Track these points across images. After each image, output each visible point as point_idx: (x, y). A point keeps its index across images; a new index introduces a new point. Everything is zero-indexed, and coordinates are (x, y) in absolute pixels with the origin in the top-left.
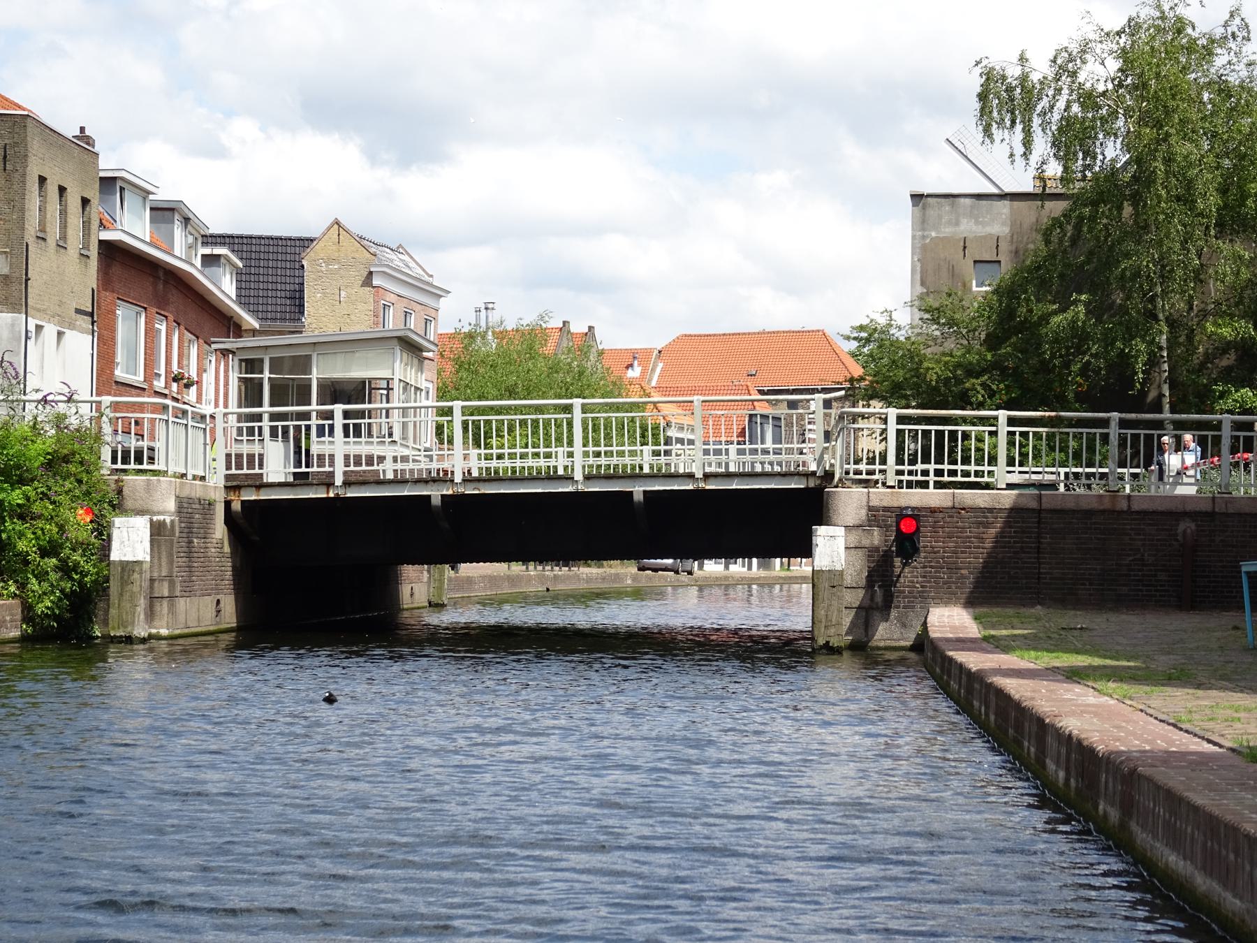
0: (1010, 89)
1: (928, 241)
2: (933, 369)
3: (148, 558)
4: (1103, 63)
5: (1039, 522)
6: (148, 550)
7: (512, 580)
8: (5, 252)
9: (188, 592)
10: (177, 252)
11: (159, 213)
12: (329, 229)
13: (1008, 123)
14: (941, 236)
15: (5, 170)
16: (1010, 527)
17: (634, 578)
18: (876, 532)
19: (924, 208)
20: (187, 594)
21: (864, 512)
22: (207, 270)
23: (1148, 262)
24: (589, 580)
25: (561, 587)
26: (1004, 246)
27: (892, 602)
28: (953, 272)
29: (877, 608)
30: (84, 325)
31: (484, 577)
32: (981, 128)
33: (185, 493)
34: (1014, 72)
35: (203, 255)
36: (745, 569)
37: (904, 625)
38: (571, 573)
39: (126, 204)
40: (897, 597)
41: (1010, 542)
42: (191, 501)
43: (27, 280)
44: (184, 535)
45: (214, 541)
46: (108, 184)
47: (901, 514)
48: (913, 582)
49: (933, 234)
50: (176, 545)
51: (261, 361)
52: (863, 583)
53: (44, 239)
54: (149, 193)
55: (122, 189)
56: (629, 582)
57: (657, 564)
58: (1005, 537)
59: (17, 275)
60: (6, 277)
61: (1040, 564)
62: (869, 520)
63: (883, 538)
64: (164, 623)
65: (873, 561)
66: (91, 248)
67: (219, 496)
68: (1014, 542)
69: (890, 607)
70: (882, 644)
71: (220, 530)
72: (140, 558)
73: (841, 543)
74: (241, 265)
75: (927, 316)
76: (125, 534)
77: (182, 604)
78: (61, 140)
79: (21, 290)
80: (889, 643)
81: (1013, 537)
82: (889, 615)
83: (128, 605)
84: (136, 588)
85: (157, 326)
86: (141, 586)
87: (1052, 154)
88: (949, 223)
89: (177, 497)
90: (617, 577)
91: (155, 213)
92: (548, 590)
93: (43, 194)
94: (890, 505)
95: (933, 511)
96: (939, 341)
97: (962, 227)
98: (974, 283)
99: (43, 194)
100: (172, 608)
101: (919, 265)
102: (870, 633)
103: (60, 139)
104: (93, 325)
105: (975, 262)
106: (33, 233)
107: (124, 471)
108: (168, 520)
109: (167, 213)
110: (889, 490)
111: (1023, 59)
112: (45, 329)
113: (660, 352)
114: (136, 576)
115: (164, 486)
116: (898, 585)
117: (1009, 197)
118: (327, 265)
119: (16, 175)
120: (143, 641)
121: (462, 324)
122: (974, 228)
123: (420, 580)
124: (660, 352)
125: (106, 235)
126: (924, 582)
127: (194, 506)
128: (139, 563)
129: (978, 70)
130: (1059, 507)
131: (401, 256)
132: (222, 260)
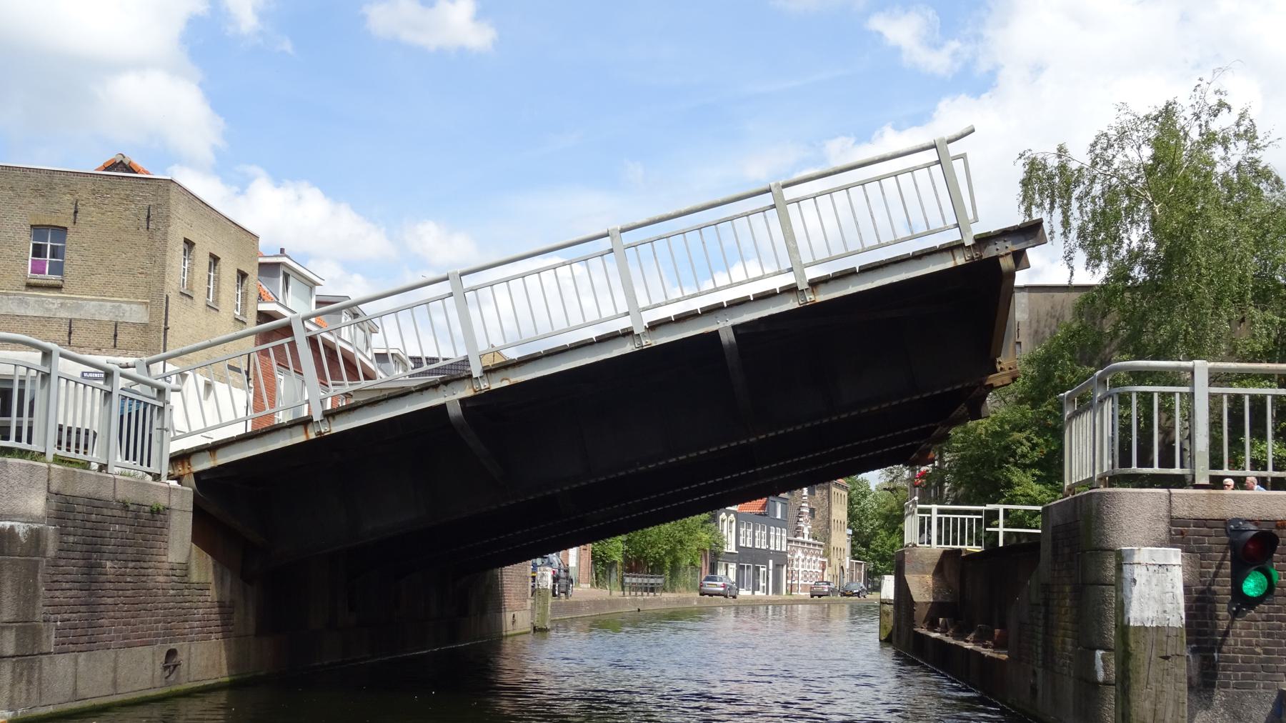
0: (1051, 177)
7: (612, 603)
8: (146, 303)
13: (1047, 206)
15: (148, 228)
17: (699, 601)
23: (1187, 326)
24: (668, 602)
27: (1215, 676)
31: (589, 602)
32: (1023, 208)
33: (85, 486)
34: (1053, 162)
36: (765, 594)
38: (656, 598)
39: (290, 287)
40: (1225, 669)
43: (166, 329)
48: (1249, 644)
53: (191, 297)
54: (315, 284)
55: (286, 276)
56: (695, 603)
57: (712, 591)
59: (156, 323)
60: (146, 325)
66: (248, 315)
69: (1213, 685)
78: (214, 215)
79: (159, 338)
82: (1210, 699)
87: (1078, 244)
90: (687, 600)
92: (639, 610)
93: (191, 257)
94: (1207, 515)
103: (213, 213)
106: (175, 287)
108: (21, 528)
111: (1061, 151)
116: (1225, 648)
117: (1027, 289)
119: (159, 233)
123: (522, 608)
129: (1022, 161)
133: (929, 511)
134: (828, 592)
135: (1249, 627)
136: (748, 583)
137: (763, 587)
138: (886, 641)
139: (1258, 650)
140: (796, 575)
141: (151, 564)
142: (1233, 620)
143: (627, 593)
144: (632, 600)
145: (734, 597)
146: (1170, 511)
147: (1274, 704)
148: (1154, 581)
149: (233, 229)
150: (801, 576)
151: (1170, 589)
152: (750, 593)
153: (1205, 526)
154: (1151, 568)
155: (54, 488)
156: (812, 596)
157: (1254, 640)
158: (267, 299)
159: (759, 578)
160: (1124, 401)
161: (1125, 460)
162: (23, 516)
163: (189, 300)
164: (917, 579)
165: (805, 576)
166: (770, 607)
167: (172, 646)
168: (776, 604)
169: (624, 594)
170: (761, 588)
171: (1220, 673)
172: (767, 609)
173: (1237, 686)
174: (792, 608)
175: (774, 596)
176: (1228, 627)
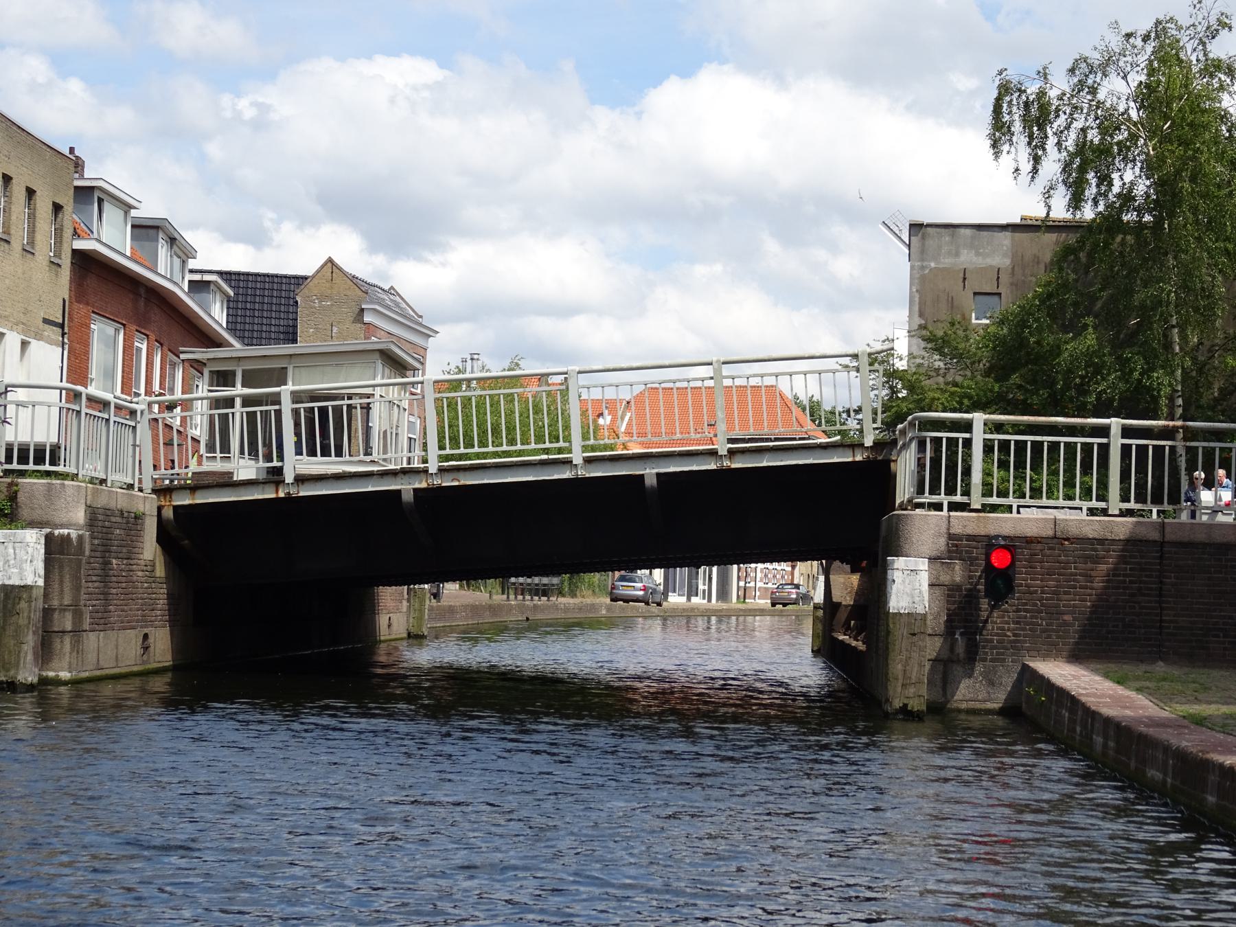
1: (927, 272)
2: (939, 399)
3: (41, 582)
4: (1125, 77)
5: (1161, 558)
6: (42, 572)
7: (494, 609)
9: (102, 623)
10: (161, 270)
11: (143, 231)
12: (322, 267)
14: (941, 266)
16: (1126, 563)
17: (609, 609)
18: (958, 566)
19: (923, 238)
20: (101, 627)
21: (942, 541)
22: (197, 296)
25: (539, 616)
26: (1005, 278)
27: (977, 653)
28: (952, 304)
29: (958, 661)
30: (53, 337)
31: (465, 607)
33: (101, 502)
35: (190, 281)
36: (705, 601)
37: (991, 683)
38: (550, 603)
39: (104, 216)
40: (984, 647)
41: (1124, 582)
42: (109, 513)
44: (98, 554)
45: (142, 562)
46: (85, 194)
47: (990, 543)
48: (1003, 629)
49: (933, 265)
50: (84, 566)
51: (233, 373)
52: (941, 628)
53: (8, 242)
54: (131, 207)
55: (100, 201)
57: (630, 595)
58: (1119, 575)
61: (1162, 609)
62: (949, 551)
63: (966, 574)
64: (66, 665)
65: (954, 603)
67: (147, 505)
68: (1131, 582)
70: (964, 706)
71: (150, 548)
72: (29, 582)
73: (924, 579)
74: (232, 294)
75: (929, 346)
76: (11, 551)
77: (92, 640)
78: (30, 140)
80: (972, 705)
81: (1130, 575)
82: (973, 670)
83: (12, 642)
84: (22, 621)
85: (136, 344)
86: (29, 618)
87: (1060, 180)
88: (949, 253)
89: (88, 507)
90: (593, 607)
91: (137, 231)
92: (528, 619)
93: (8, 194)
95: (1029, 541)
96: (941, 372)
97: (962, 258)
98: (973, 315)
99: (8, 194)
100: (77, 647)
101: (917, 296)
102: (948, 694)
103: (29, 138)
104: (63, 337)
105: (975, 294)
107: (22, 474)
108: (74, 534)
109: (152, 232)
110: (974, 514)
112: (6, 337)
113: (628, 403)
114: (23, 605)
115: (69, 491)
116: (985, 632)
117: (1010, 229)
118: (320, 302)
120: (31, 688)
121: (450, 367)
122: (975, 259)
123: (398, 610)
124: (628, 403)
125: (79, 245)
126: (1017, 629)
127: (113, 519)
128: (27, 588)
130: (1186, 540)
131: (392, 297)
132: (212, 287)
133: (967, 426)
134: (796, 599)
135: (1003, 617)
136: (681, 587)
137: (704, 591)
138: (816, 652)
139: (1009, 633)
140: (752, 574)
141: (135, 561)
142: (991, 612)
143: (512, 597)
144: (518, 605)
145: (659, 604)
146: (948, 529)
147: (1019, 674)
148: (907, 581)
149: (49, 153)
150: (759, 575)
151: (917, 587)
152: (683, 599)
153: (974, 541)
154: (906, 572)
155: (88, 503)
156: (773, 605)
157: (1006, 626)
158: (82, 234)
159: (697, 579)
160: (922, 444)
161: (920, 491)
162: (75, 525)
163: (6, 245)
164: (842, 580)
165: (766, 576)
166: (714, 619)
167: (146, 630)
168: (722, 616)
169: (508, 597)
170: (700, 593)
171: (981, 651)
172: (709, 622)
173: (992, 660)
174: (745, 621)
175: (720, 604)
176: (988, 617)
